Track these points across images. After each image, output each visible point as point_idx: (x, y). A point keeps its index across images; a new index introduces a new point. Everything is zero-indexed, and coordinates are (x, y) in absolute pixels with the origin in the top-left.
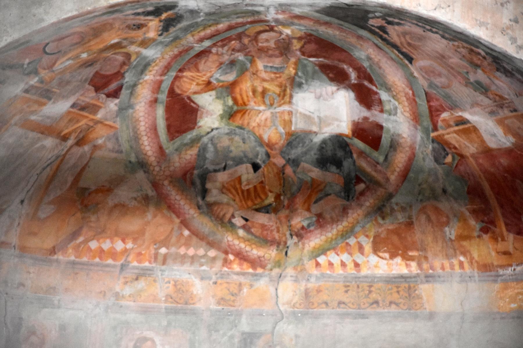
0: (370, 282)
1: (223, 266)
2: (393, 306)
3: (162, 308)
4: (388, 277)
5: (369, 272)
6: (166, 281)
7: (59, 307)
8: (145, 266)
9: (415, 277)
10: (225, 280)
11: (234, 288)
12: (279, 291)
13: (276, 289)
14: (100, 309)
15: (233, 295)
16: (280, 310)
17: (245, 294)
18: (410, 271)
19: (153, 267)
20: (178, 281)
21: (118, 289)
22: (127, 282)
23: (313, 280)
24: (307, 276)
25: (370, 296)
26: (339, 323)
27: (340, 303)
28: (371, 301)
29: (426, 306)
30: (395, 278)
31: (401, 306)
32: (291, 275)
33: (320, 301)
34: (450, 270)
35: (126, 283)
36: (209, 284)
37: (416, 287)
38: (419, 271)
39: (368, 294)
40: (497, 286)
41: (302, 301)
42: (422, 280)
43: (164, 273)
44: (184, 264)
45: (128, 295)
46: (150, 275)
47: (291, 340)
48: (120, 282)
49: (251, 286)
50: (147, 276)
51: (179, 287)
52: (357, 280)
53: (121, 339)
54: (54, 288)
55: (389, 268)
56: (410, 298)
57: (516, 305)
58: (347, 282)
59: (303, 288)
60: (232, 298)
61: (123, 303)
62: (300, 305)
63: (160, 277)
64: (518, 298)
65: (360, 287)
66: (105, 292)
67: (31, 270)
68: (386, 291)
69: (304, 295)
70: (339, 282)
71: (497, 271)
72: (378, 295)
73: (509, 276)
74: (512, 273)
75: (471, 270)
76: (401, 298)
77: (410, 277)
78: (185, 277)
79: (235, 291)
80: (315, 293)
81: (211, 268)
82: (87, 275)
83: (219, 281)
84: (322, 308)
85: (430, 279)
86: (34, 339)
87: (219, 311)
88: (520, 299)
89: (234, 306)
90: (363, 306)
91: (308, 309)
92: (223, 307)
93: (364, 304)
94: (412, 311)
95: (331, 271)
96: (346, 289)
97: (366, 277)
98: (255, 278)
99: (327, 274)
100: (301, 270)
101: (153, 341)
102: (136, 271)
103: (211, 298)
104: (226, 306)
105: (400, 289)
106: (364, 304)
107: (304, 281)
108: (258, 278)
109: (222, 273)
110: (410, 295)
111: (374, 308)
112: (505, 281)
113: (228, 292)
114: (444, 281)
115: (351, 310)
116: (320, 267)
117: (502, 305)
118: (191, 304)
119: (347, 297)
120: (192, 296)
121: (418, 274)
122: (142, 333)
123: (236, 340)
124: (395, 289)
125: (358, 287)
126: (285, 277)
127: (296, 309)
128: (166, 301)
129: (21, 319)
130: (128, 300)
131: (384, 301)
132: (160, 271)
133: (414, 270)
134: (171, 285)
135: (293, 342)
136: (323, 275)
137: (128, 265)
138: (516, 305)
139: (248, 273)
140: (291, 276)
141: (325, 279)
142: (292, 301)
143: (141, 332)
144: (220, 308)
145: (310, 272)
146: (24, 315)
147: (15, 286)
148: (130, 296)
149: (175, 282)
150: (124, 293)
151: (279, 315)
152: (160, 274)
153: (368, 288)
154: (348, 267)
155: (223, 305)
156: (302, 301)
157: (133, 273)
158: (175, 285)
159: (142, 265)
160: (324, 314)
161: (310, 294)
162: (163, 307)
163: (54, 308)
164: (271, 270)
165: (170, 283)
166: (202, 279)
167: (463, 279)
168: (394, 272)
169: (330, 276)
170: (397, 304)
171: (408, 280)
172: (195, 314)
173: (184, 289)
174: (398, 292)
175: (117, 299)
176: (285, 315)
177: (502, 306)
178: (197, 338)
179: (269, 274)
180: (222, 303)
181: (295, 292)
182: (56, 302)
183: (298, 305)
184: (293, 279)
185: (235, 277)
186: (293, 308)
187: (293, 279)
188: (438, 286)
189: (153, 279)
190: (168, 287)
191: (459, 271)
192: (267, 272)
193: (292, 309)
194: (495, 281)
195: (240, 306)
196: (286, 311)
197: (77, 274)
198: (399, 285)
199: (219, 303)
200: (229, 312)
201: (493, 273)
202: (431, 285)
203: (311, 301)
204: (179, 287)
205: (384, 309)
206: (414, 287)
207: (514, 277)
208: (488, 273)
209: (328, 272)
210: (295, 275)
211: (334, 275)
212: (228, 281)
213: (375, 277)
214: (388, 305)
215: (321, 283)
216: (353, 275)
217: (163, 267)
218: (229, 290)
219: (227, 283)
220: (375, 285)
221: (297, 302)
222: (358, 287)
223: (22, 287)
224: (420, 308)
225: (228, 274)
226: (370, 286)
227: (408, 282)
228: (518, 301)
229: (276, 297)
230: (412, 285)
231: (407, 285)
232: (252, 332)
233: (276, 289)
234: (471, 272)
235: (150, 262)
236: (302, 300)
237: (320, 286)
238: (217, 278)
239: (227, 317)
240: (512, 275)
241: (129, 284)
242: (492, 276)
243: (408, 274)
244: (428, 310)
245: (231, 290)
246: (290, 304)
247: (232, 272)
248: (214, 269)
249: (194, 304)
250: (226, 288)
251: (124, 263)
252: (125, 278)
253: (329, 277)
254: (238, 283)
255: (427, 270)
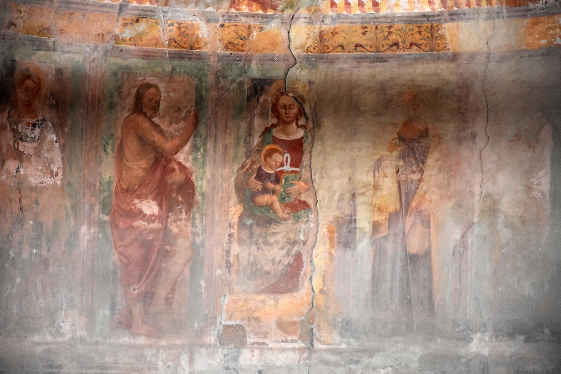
0: (389, 23)
1: (231, 7)
2: (414, 48)
3: (166, 53)
4: (410, 17)
5: (389, 11)
6: (168, 23)
7: (54, 50)
8: (146, 7)
9: (438, 16)
10: (233, 23)
11: (243, 31)
12: (291, 34)
13: (289, 32)
14: (99, 53)
15: (242, 39)
16: (292, 54)
17: (254, 38)
18: (434, 9)
19: (154, 7)
20: (182, 23)
21: (117, 31)
22: (127, 24)
23: (328, 21)
24: (321, 17)
25: (389, 37)
26: (357, 68)
27: (357, 46)
28: (391, 43)
29: (449, 46)
30: (417, 17)
31: (423, 47)
32: (305, 16)
33: (336, 45)
34: (476, 7)
35: (125, 25)
36: (216, 27)
37: (440, 26)
38: (443, 9)
39: (388, 36)
40: (526, 22)
41: (316, 45)
42: (445, 19)
43: (167, 14)
44: (188, 5)
45: (128, 38)
46: (151, 17)
47: (305, 86)
48: (119, 24)
49: (261, 29)
50: (148, 18)
51: (183, 30)
52: (375, 20)
53: (123, 84)
54: (48, 29)
55: (411, 6)
56: (432, 38)
57: (546, 41)
58: (365, 23)
59: (317, 31)
60: (241, 42)
61: (124, 46)
62: (314, 49)
63: (162, 18)
64: (549, 33)
65: (379, 27)
66: (103, 35)
67: (22, 9)
68: (407, 31)
69: (318, 38)
70: (357, 23)
71: (528, 5)
72: (398, 36)
73: (540, 10)
74: (543, 6)
75: (499, 5)
76: (422, 39)
77: (433, 16)
78: (189, 19)
79: (245, 35)
80: (330, 35)
81: (218, 9)
82: (84, 15)
83: (227, 24)
84: (338, 52)
85: (455, 17)
86: (29, 83)
87: (227, 56)
88: (550, 35)
89: (243, 51)
90: (381, 49)
91: (322, 53)
92: (231, 52)
93: (383, 47)
94: (434, 53)
95: (347, 12)
96: (363, 31)
97: (386, 17)
98: (265, 20)
99: (344, 15)
100: (315, 11)
101: (157, 88)
102: (136, 12)
103: (218, 42)
104: (234, 50)
105: (422, 29)
106: (383, 47)
107: (319, 23)
108: (269, 20)
109: (230, 14)
110: (432, 36)
111: (394, 50)
112: (535, 16)
113: (237, 35)
114: (469, 19)
115: (369, 53)
116: (336, 7)
117: (531, 41)
118: (197, 49)
119: (365, 40)
120: (197, 40)
121: (441, 12)
122: (145, 79)
123: (246, 87)
124: (416, 30)
125: (377, 28)
126: (298, 18)
127: (310, 54)
128: (170, 45)
129: (13, 61)
130: (128, 44)
131: (404, 43)
132: (162, 12)
133: (437, 8)
134: (174, 28)
135: (307, 88)
136: (339, 16)
137: (127, 6)
138: (546, 41)
139: (258, 15)
140: (305, 18)
141: (341, 20)
142: (305, 45)
143: (143, 78)
144: (228, 52)
145: (325, 13)
146: (17, 58)
147: (6, 25)
148: (130, 39)
149: (179, 24)
150: (124, 36)
151: (292, 60)
152: (162, 16)
153: (387, 30)
154: (366, 7)
155: (231, 49)
156: (316, 45)
157: (133, 14)
158: (179, 28)
159: (141, 6)
160: (339, 59)
161: (325, 37)
162: (167, 52)
163: (49, 51)
164: (283, 11)
165: (173, 25)
166: (208, 21)
167: (490, 16)
168: (416, 11)
169: (346, 17)
170: (418, 46)
171: (431, 19)
172: (200, 59)
173: (189, 33)
174: (420, 32)
175: (117, 42)
176: (298, 60)
177: (531, 43)
178: (204, 84)
179: (281, 16)
180: (230, 47)
181: (309, 35)
182: (51, 44)
183: (311, 49)
184: (307, 20)
185: (244, 19)
186: (307, 53)
187: (307, 20)
188: (463, 24)
189: (155, 21)
190: (171, 31)
191: (486, 7)
192: (278, 14)
193: (305, 54)
194: (524, 16)
195: (249, 50)
196: (299, 56)
197: (71, 14)
198: (421, 25)
199: (226, 48)
200: (238, 57)
201: (522, 8)
202: (455, 24)
203: (326, 44)
204: (183, 30)
205: (404, 51)
206: (437, 26)
207: (545, 11)
208: (518, 8)
209: (345, 13)
210: (308, 16)
211: (351, 15)
212: (236, 24)
213: (395, 17)
214: (408, 47)
215: (337, 25)
216: (371, 16)
217: (166, 8)
218: (237, 33)
219: (235, 25)
220: (396, 26)
221: (311, 46)
222: (377, 28)
223: (13, 27)
224: (442, 49)
225: (236, 16)
226: (390, 27)
227: (431, 21)
228: (548, 36)
229: (288, 41)
230: (435, 25)
231: (429, 25)
232: (263, 78)
233: (289, 32)
234: (499, 8)
235: (151, 2)
236: (316, 43)
237: (335, 28)
238: (224, 21)
239: (236, 63)
240: (543, 9)
241: (128, 26)
242: (521, 11)
243: (430, 12)
244: (451, 51)
245: (239, 34)
246: (304, 47)
247: (241, 14)
248: (220, 11)
249: (200, 48)
250: (234, 31)
251: (123, 3)
252: (124, 19)
253: (346, 18)
254: (247, 26)
255: (452, 7)
